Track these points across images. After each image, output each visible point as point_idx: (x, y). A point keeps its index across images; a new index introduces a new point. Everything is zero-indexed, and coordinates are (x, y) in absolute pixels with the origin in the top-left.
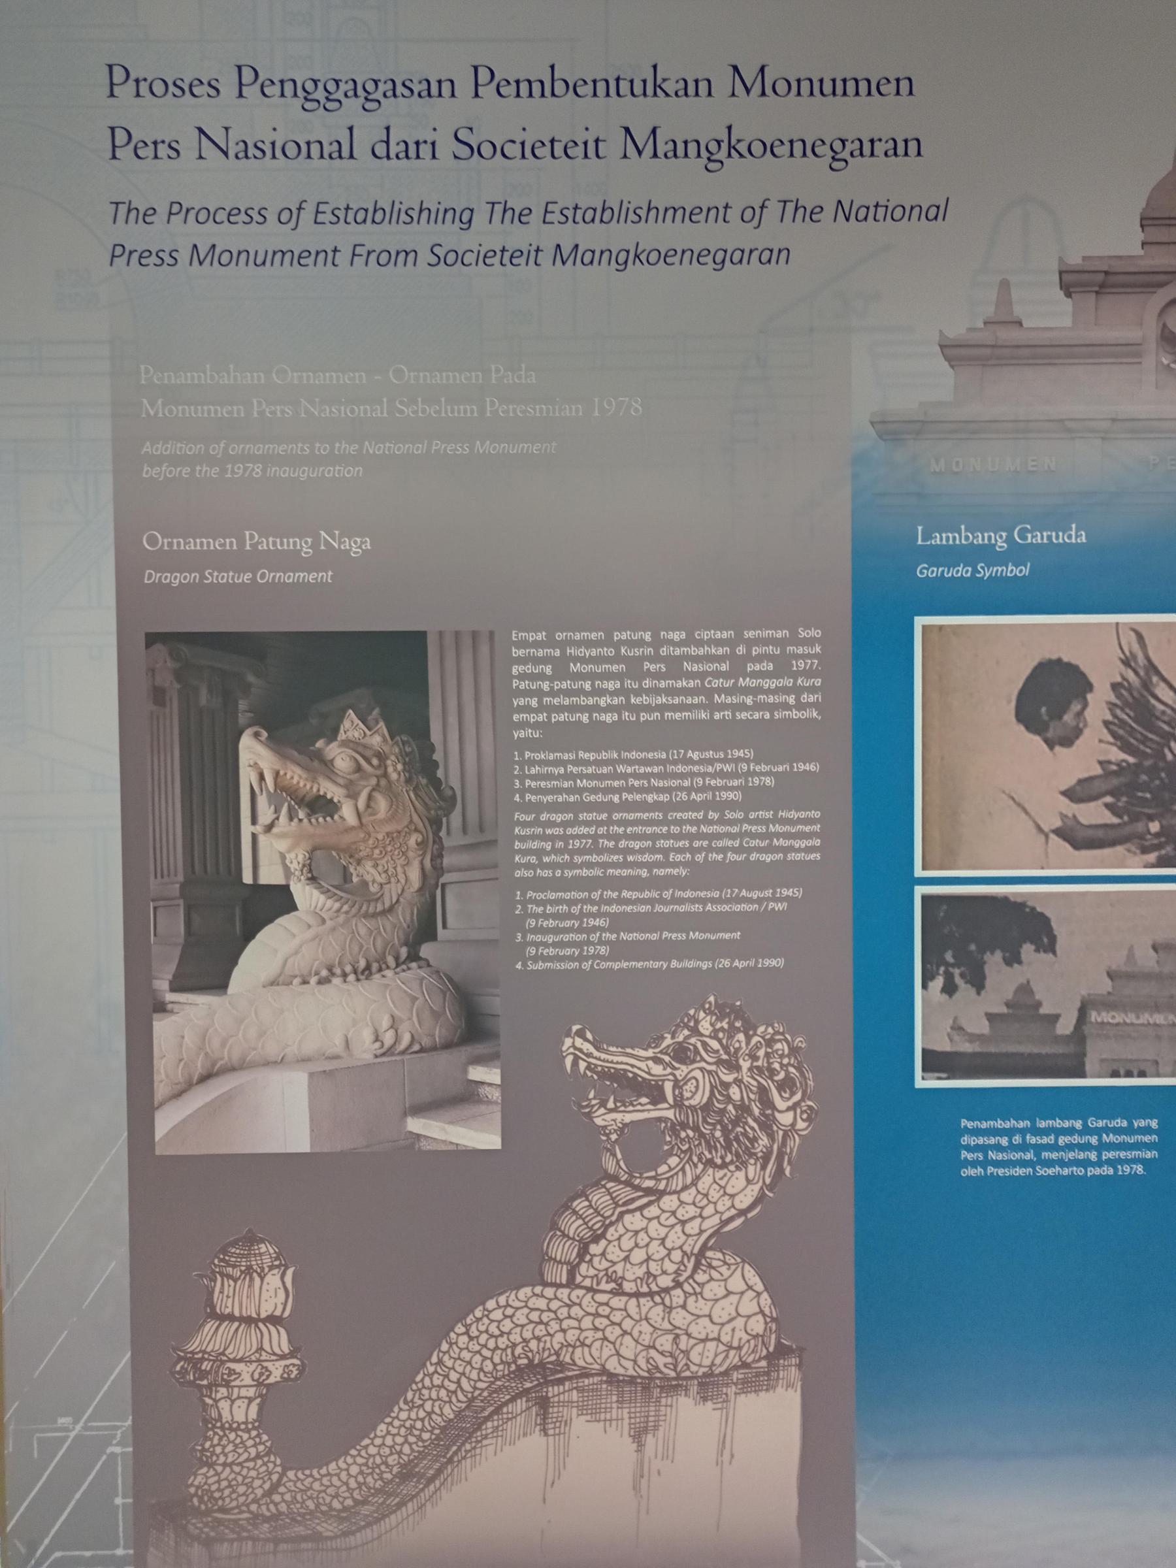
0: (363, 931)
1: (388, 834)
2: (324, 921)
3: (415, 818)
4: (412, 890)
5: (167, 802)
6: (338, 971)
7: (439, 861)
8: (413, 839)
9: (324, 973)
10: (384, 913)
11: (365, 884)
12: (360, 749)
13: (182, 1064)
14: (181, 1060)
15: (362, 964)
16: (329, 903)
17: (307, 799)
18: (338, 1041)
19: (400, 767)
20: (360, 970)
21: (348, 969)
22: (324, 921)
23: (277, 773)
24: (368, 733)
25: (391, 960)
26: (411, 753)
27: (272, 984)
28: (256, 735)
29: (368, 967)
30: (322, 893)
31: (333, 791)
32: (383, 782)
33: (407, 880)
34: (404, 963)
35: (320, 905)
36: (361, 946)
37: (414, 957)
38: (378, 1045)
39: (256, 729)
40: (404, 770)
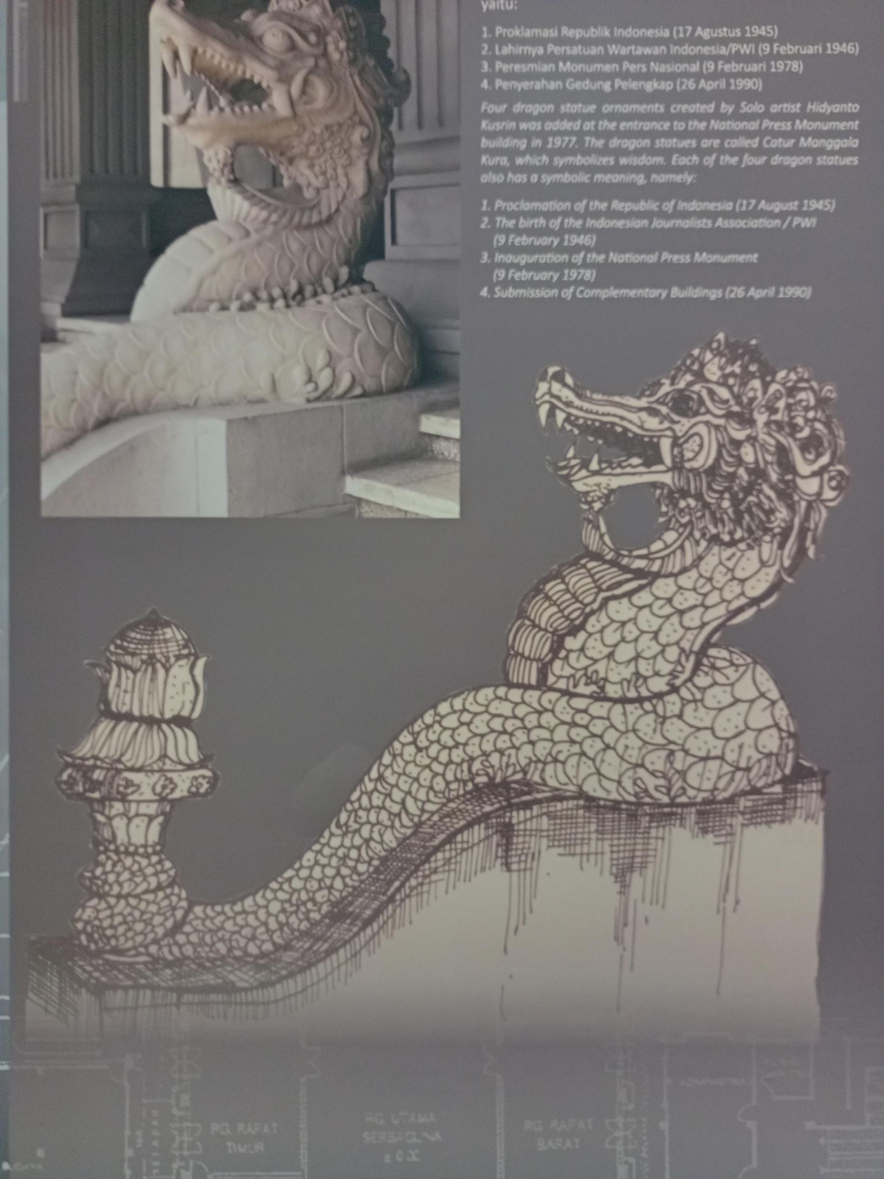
0: (295, 246)
1: (327, 127)
2: (247, 234)
3: (361, 107)
4: (355, 197)
8: (358, 134)
9: (247, 297)
10: (321, 224)
12: (296, 23)
15: (293, 287)
16: (255, 211)
18: (263, 382)
19: (342, 45)
21: (276, 292)
22: (247, 234)
25: (328, 282)
29: (300, 291)
30: (246, 198)
31: (259, 73)
33: (349, 184)
36: (292, 266)
37: (356, 279)
38: (311, 387)
40: (348, 48)
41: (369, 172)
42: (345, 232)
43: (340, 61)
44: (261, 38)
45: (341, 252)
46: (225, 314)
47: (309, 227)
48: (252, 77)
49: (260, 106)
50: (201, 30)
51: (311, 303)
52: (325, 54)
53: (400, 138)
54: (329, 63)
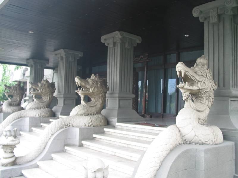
1: (97, 94)
5: (234, 77)
8: (48, 94)
10: (44, 102)
18: (34, 115)
19: (100, 84)
28: (78, 78)
31: (88, 87)
39: (77, 77)
44: (89, 82)
51: (41, 109)
52: (45, 87)
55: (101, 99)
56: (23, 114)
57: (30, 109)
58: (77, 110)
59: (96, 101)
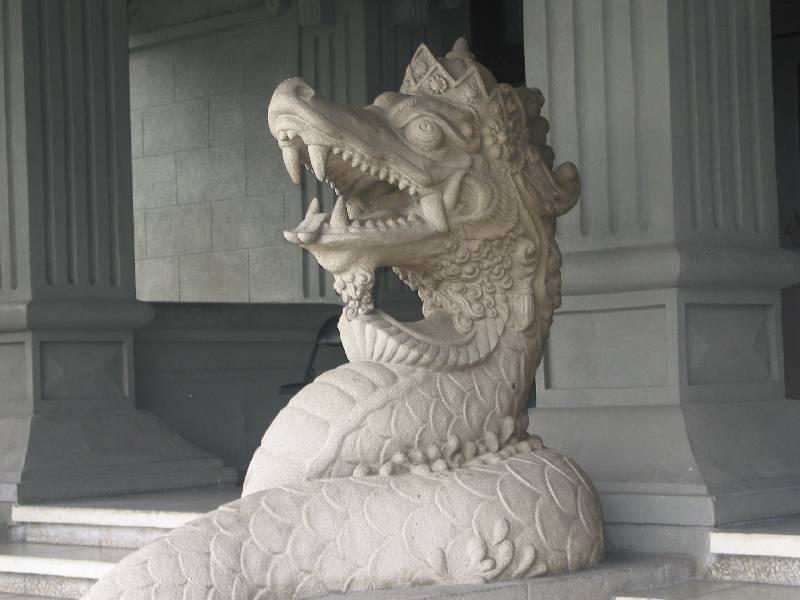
0: (451, 395)
1: (487, 241)
2: (394, 378)
3: (525, 214)
4: (517, 328)
6: (418, 455)
7: (555, 282)
8: (522, 249)
9: (398, 458)
11: (446, 320)
12: (444, 111)
13: (213, 590)
14: (210, 587)
15: (452, 443)
16: (402, 350)
17: (360, 186)
18: (433, 559)
19: (502, 138)
20: (449, 453)
21: (432, 452)
22: (394, 378)
23: (329, 150)
24: (453, 83)
25: (490, 437)
26: (514, 113)
27: (321, 475)
28: (297, 93)
29: (459, 450)
30: (391, 334)
31: (405, 177)
32: (479, 161)
33: (510, 313)
34: (508, 442)
35: (387, 353)
36: (450, 418)
37: (521, 434)
38: (487, 564)
40: (507, 142)
41: (534, 296)
42: (507, 375)
43: (500, 157)
45: (505, 401)
46: (373, 477)
47: (467, 368)
48: (397, 181)
49: (405, 217)
50: (337, 128)
53: (564, 248)
54: (487, 163)
55: (524, 287)
56: (266, 562)
57: (331, 470)
58: (326, 424)
59: (488, 309)
